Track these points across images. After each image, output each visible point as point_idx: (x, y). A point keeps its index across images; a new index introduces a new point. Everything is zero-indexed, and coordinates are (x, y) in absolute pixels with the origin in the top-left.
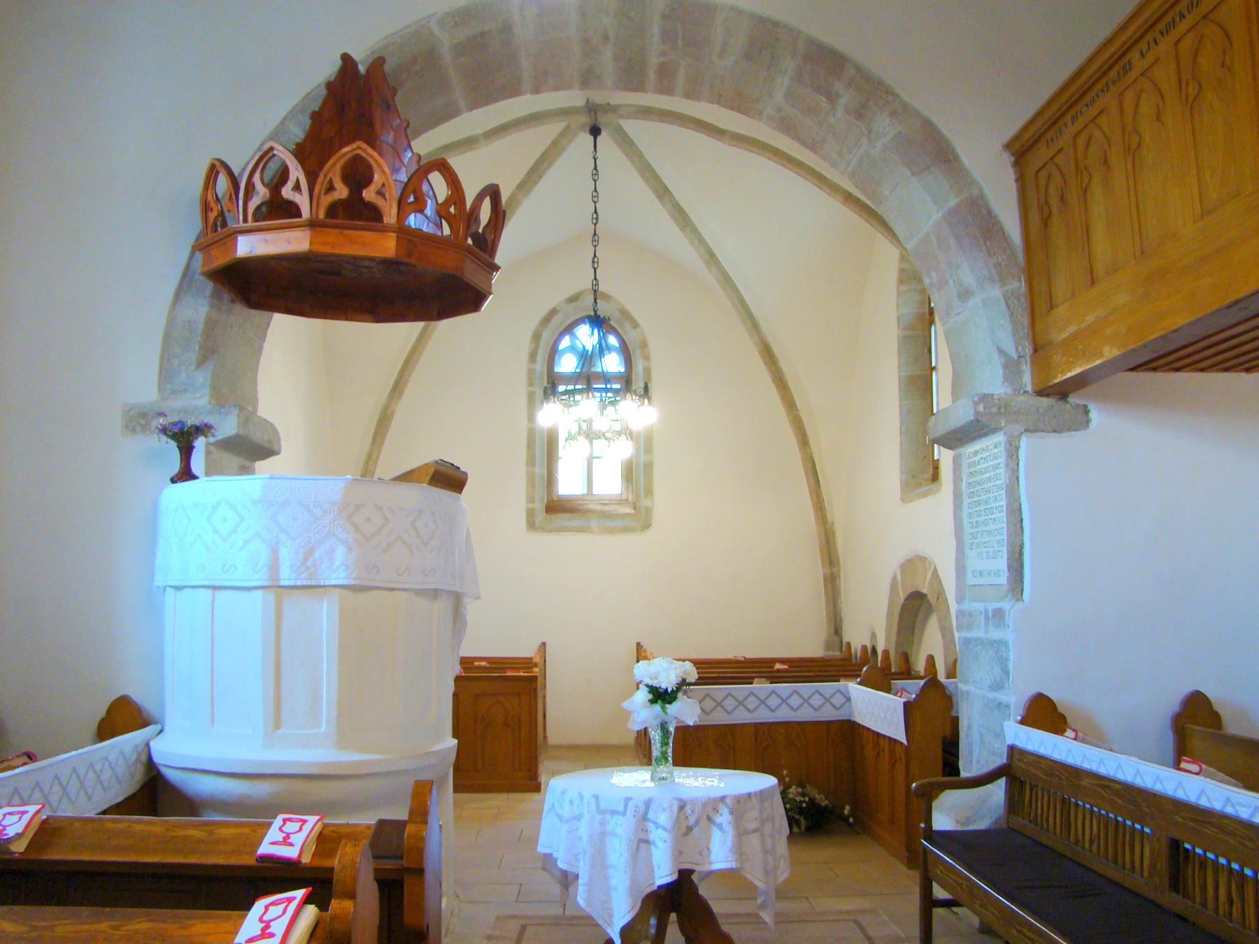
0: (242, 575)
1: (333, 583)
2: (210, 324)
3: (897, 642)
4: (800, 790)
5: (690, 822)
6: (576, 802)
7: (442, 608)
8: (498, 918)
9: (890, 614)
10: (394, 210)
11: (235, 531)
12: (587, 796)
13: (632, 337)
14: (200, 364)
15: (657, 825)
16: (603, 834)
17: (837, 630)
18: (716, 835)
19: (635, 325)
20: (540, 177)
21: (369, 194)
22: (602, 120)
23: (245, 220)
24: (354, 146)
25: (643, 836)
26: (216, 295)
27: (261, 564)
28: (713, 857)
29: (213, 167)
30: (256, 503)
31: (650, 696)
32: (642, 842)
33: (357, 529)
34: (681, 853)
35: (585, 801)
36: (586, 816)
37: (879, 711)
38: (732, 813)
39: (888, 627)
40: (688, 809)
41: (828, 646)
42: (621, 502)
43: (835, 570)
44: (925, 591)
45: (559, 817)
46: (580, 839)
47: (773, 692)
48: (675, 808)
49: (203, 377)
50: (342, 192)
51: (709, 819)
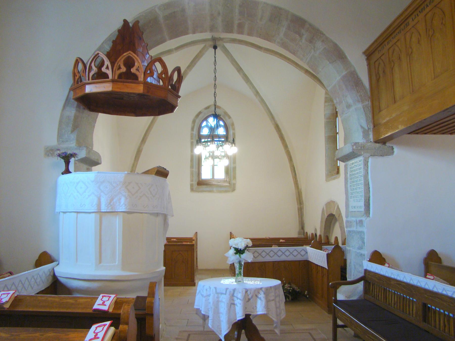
0: (88, 208)
1: (120, 210)
2: (76, 117)
3: (324, 232)
4: (289, 285)
5: (250, 297)
6: (208, 290)
7: (159, 220)
9: (321, 222)
10: (143, 76)
11: (85, 192)
12: (212, 287)
13: (228, 122)
14: (72, 131)
15: (238, 298)
16: (218, 301)
17: (303, 228)
18: (259, 302)
19: (230, 117)
20: (195, 64)
21: (133, 70)
22: (218, 43)
23: (89, 80)
24: (128, 53)
25: (232, 302)
26: (78, 107)
27: (94, 204)
28: (258, 309)
29: (77, 60)
30: (93, 182)
31: (235, 252)
32: (232, 304)
33: (129, 191)
34: (246, 308)
35: (211, 289)
36: (212, 295)
38: (264, 294)
40: (249, 292)
41: (299, 233)
42: (224, 181)
43: (302, 206)
44: (334, 213)
45: (202, 295)
46: (210, 303)
47: (279, 250)
48: (244, 292)
49: (73, 136)
50: (124, 69)
51: (256, 296)
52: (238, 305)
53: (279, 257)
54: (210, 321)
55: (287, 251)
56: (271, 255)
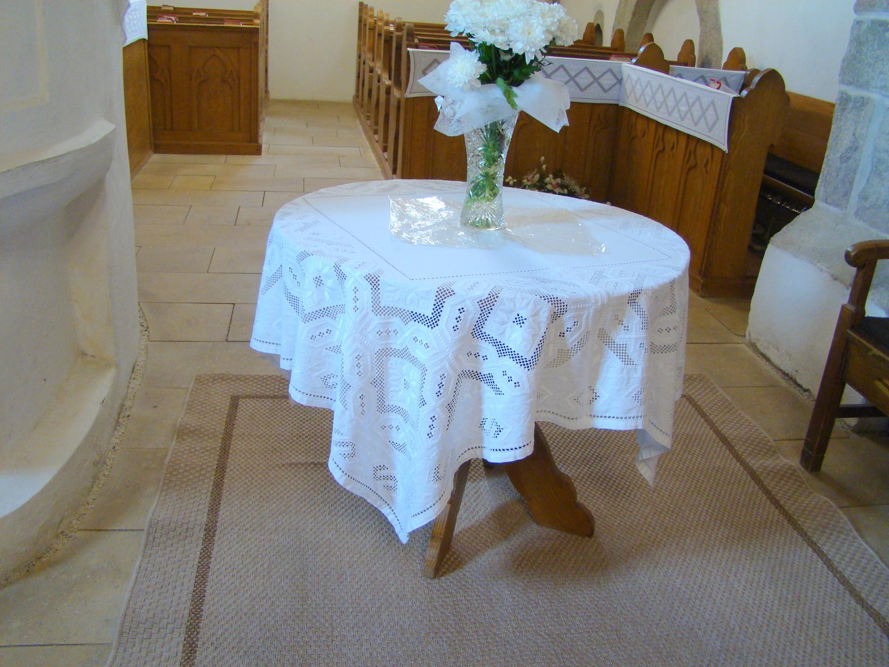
4: (559, 180)
5: (567, 339)
6: (329, 283)
12: (355, 277)
15: (503, 350)
25: (468, 365)
28: (600, 405)
31: (483, 68)
32: (468, 376)
35: (349, 284)
37: (698, 109)
40: (567, 319)
45: (294, 301)
46: (337, 350)
47: (562, 66)
48: (544, 315)
52: (501, 382)
54: (335, 450)
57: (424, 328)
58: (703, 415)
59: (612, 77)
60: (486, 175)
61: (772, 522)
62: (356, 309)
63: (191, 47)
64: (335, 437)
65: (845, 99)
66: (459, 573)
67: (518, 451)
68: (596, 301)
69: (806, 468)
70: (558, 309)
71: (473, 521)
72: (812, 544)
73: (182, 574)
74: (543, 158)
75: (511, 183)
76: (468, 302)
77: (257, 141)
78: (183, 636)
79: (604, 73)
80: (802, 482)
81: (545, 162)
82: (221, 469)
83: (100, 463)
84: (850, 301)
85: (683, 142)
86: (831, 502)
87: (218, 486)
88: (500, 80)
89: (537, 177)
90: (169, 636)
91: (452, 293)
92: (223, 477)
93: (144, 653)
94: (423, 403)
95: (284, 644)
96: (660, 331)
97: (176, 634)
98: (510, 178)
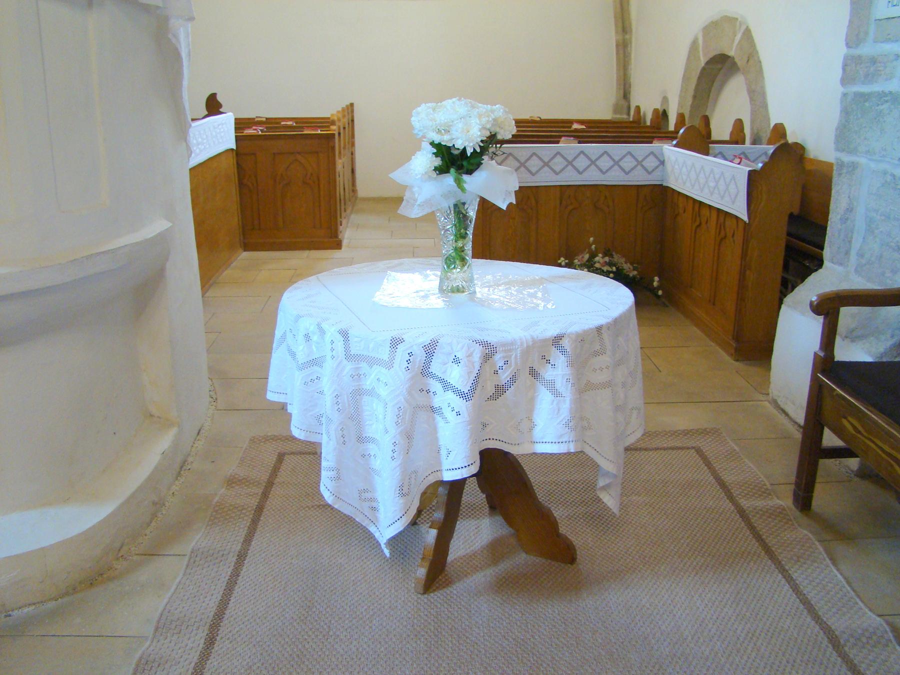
3: (692, 106)
4: (607, 259)
5: (499, 378)
6: (315, 338)
8: (253, 440)
9: (686, 78)
12: (331, 332)
15: (446, 386)
16: (358, 393)
17: (626, 96)
18: (545, 401)
28: (537, 433)
31: (438, 162)
32: (418, 411)
34: (485, 425)
35: (328, 338)
36: (329, 365)
37: (716, 182)
38: (571, 364)
39: (684, 90)
41: (616, 110)
43: (627, 37)
44: (731, 53)
45: (293, 355)
47: (582, 152)
51: (534, 373)
53: (580, 173)
54: (324, 474)
55: (605, 157)
56: (557, 168)
57: (384, 370)
58: (708, 464)
59: (654, 159)
60: (456, 249)
61: (749, 552)
62: (333, 357)
63: (274, 154)
64: (324, 464)
65: (841, 165)
66: (448, 590)
67: (464, 469)
68: (522, 344)
69: (797, 507)
70: (489, 352)
71: (468, 551)
72: (784, 571)
73: (213, 587)
74: (592, 239)
75: (563, 264)
76: (415, 348)
77: (336, 236)
78: (206, 632)
79: (647, 156)
80: (791, 520)
81: (594, 243)
82: (260, 509)
83: (158, 504)
84: (821, 348)
85: (714, 215)
86: (810, 535)
87: (255, 522)
88: (452, 170)
89: (587, 256)
90: (195, 632)
91: (402, 341)
92: (260, 516)
93: (173, 644)
94: (387, 432)
95: (287, 640)
96: (595, 370)
97: (200, 631)
98: (562, 259)
